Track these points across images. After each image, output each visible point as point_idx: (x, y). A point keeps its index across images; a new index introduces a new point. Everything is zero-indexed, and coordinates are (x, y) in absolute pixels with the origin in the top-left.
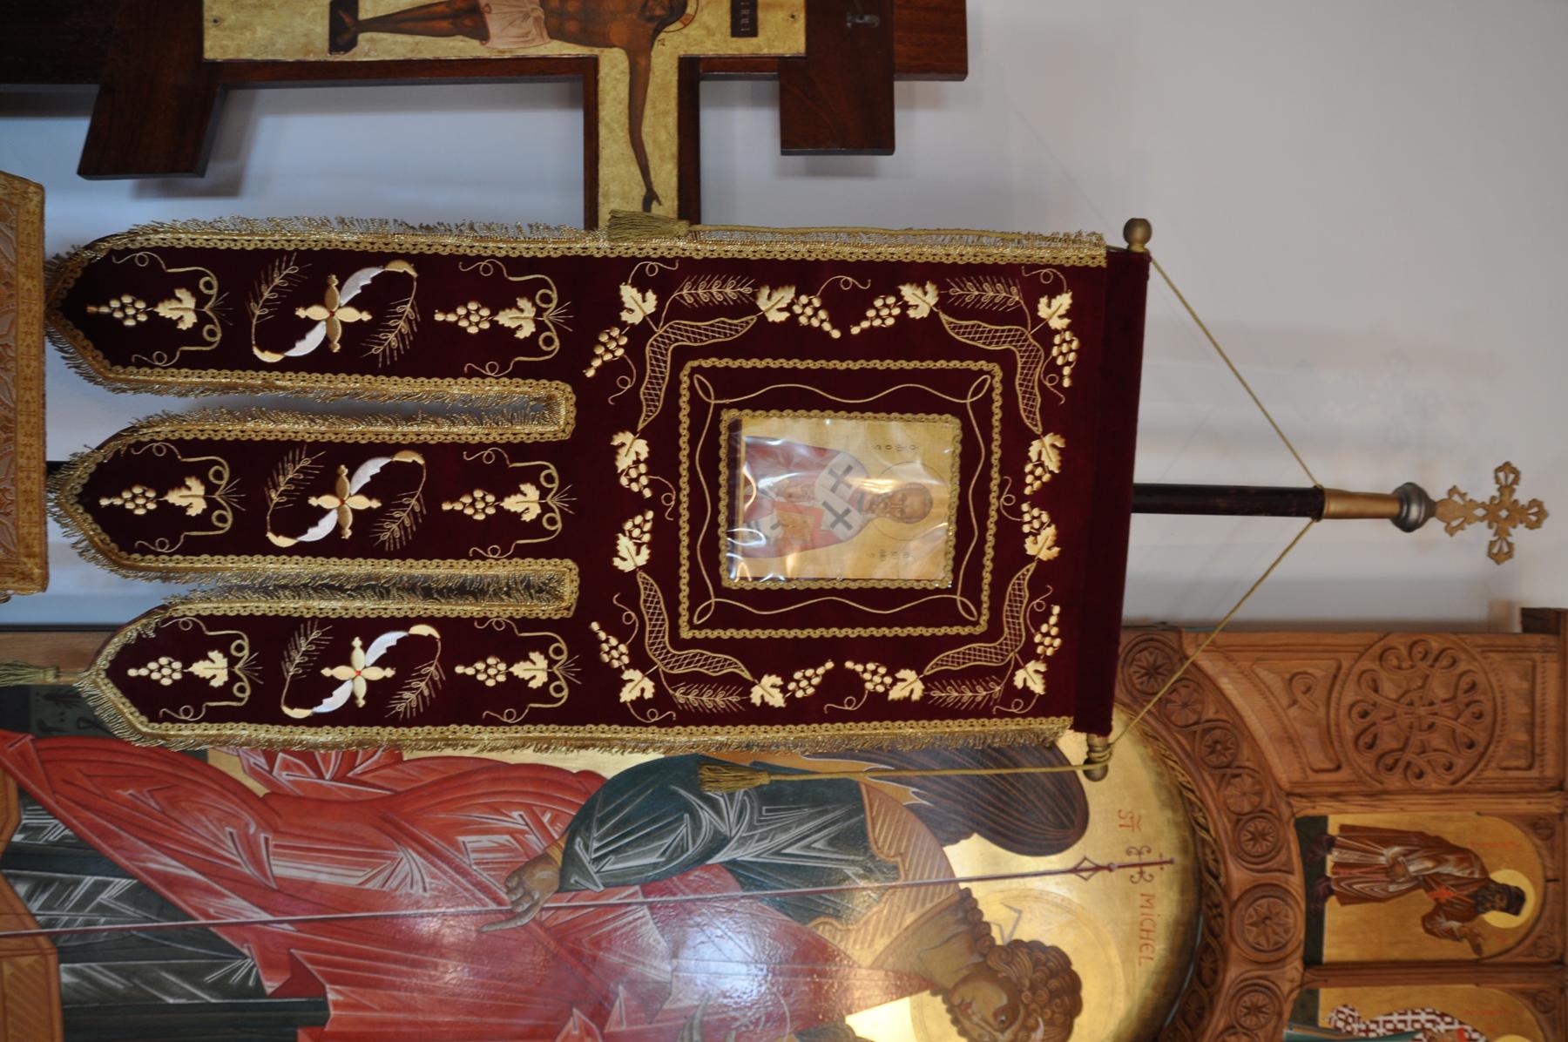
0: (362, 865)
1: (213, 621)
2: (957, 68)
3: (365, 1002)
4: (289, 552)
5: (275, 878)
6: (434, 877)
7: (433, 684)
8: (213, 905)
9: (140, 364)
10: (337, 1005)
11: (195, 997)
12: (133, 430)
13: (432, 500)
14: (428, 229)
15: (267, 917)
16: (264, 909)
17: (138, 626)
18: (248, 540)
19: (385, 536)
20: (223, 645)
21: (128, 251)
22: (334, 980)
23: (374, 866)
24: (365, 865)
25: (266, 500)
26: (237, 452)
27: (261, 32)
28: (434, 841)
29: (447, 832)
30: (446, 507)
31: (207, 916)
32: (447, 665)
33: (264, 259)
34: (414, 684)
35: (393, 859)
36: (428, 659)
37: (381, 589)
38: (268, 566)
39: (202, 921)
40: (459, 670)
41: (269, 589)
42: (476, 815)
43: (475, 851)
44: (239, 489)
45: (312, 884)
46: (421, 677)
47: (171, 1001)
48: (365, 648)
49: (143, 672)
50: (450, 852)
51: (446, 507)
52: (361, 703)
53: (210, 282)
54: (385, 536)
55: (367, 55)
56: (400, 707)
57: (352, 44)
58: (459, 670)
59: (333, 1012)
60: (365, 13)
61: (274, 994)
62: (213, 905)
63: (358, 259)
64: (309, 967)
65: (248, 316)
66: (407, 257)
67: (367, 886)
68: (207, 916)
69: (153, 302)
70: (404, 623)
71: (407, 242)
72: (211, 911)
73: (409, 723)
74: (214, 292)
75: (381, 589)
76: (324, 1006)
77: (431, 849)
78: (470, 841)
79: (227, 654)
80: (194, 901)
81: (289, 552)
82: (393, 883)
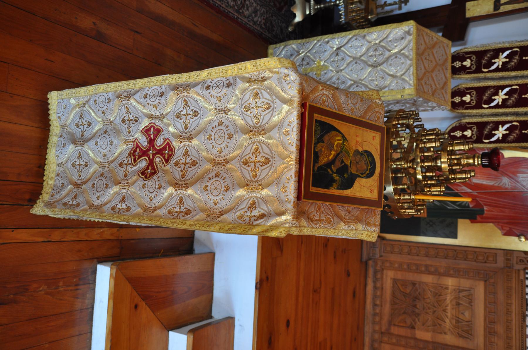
0: (493, 180)
1: (469, 123)
2: (193, 232)
3: (493, 210)
4: (487, 108)
5: (474, 183)
6: (511, 183)
7: (517, 134)
8: (459, 188)
9: (458, 74)
10: (486, 210)
11: (454, 207)
12: (458, 85)
13: (520, 95)
14: (522, 41)
15: (471, 191)
16: (470, 189)
17: (456, 123)
18: (479, 106)
19: (509, 103)
20: (470, 128)
21: (459, 53)
22: (486, 205)
23: (496, 180)
24: (494, 180)
25: (482, 98)
26: (476, 89)
27: (478, 10)
28: (511, 175)
29: (515, 173)
30: (523, 96)
31: (458, 190)
32: (521, 131)
33: (485, 52)
34: (513, 134)
35: (501, 179)
36: (516, 129)
37: (506, 114)
38: (520, 81)
39: (457, 191)
40: (523, 132)
41: (481, 116)
42: (521, 170)
43: (522, 177)
44: (477, 96)
45: (482, 184)
46: (514, 133)
47: (449, 208)
48: (502, 127)
49: (454, 134)
50: (515, 178)
51: (523, 96)
52: (500, 138)
53: (474, 57)
54: (509, 103)
55: (502, 10)
56: (510, 139)
57: (499, 9)
58: (523, 132)
59: (485, 212)
60: (502, 2)
61: (472, 207)
62: (459, 188)
63: (503, 50)
64: (481, 202)
65: (481, 63)
66: (517, 47)
67: (495, 185)
68: (458, 190)
69: (462, 62)
70: (511, 122)
71: (518, 44)
72: (459, 189)
73: (511, 143)
74: (474, 59)
75: (506, 114)
76: (483, 210)
77: (510, 177)
78: (521, 175)
79: (471, 130)
80: (455, 187)
81: (487, 108)
82: (501, 184)
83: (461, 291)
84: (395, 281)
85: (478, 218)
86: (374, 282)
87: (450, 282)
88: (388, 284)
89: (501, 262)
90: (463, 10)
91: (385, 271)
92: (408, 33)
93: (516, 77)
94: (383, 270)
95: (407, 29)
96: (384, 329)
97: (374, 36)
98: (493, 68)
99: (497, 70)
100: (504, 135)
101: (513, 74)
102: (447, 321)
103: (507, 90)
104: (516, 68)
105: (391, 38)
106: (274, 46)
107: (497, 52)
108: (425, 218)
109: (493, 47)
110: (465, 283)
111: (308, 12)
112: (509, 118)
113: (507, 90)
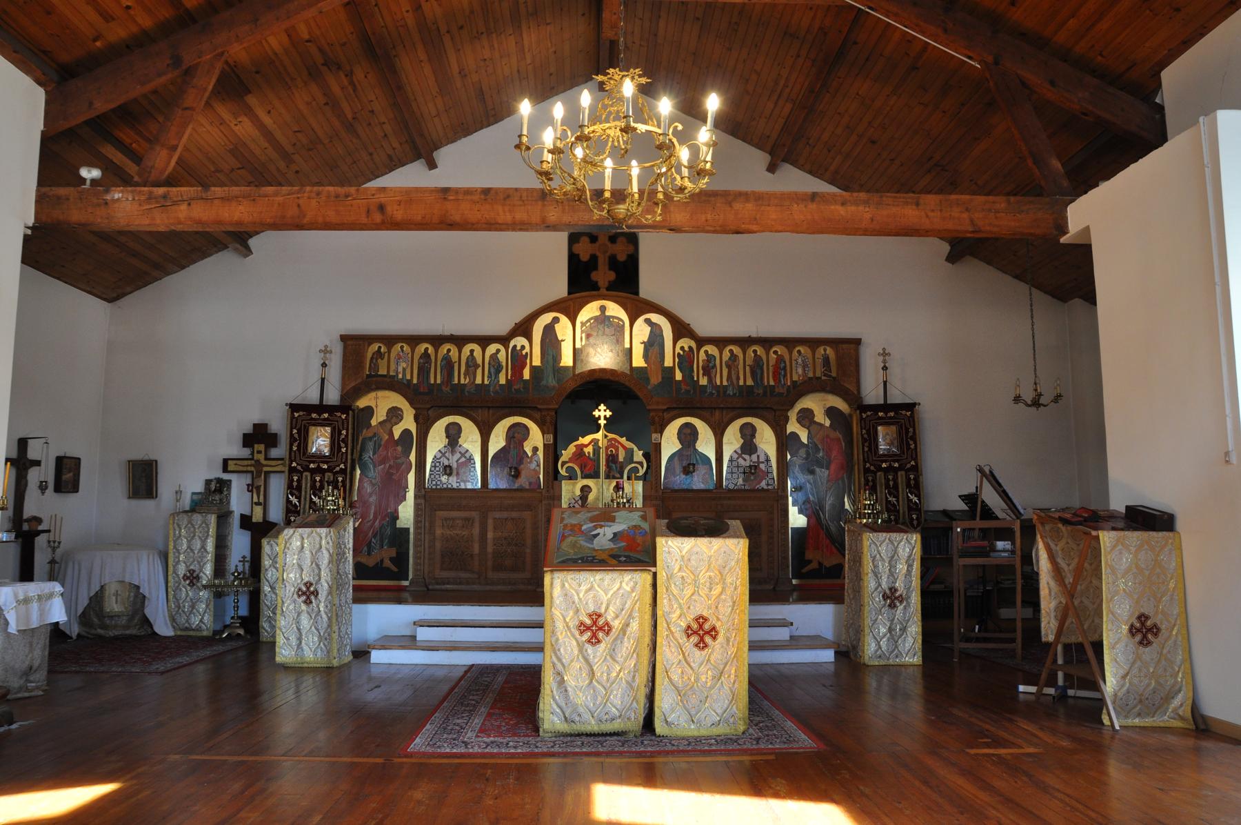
33: (287, 507)
38: (308, 490)
63: (288, 498)
71: (286, 490)
83: (443, 525)
84: (442, 569)
85: (396, 515)
86: (444, 584)
87: (438, 532)
88: (445, 574)
89: (419, 501)
90: (257, 524)
91: (436, 577)
92: (268, 543)
93: (306, 492)
94: (435, 578)
95: (266, 543)
96: (476, 576)
97: (266, 563)
98: (298, 504)
99: (299, 502)
100: (296, 498)
101: (303, 493)
102: (464, 533)
103: (313, 497)
104: (300, 491)
105: (269, 553)
106: (261, 637)
107: (288, 501)
108: (397, 549)
109: (744, 692)
110: (438, 523)
111: (238, 625)
112: (308, 496)
113: (313, 497)
